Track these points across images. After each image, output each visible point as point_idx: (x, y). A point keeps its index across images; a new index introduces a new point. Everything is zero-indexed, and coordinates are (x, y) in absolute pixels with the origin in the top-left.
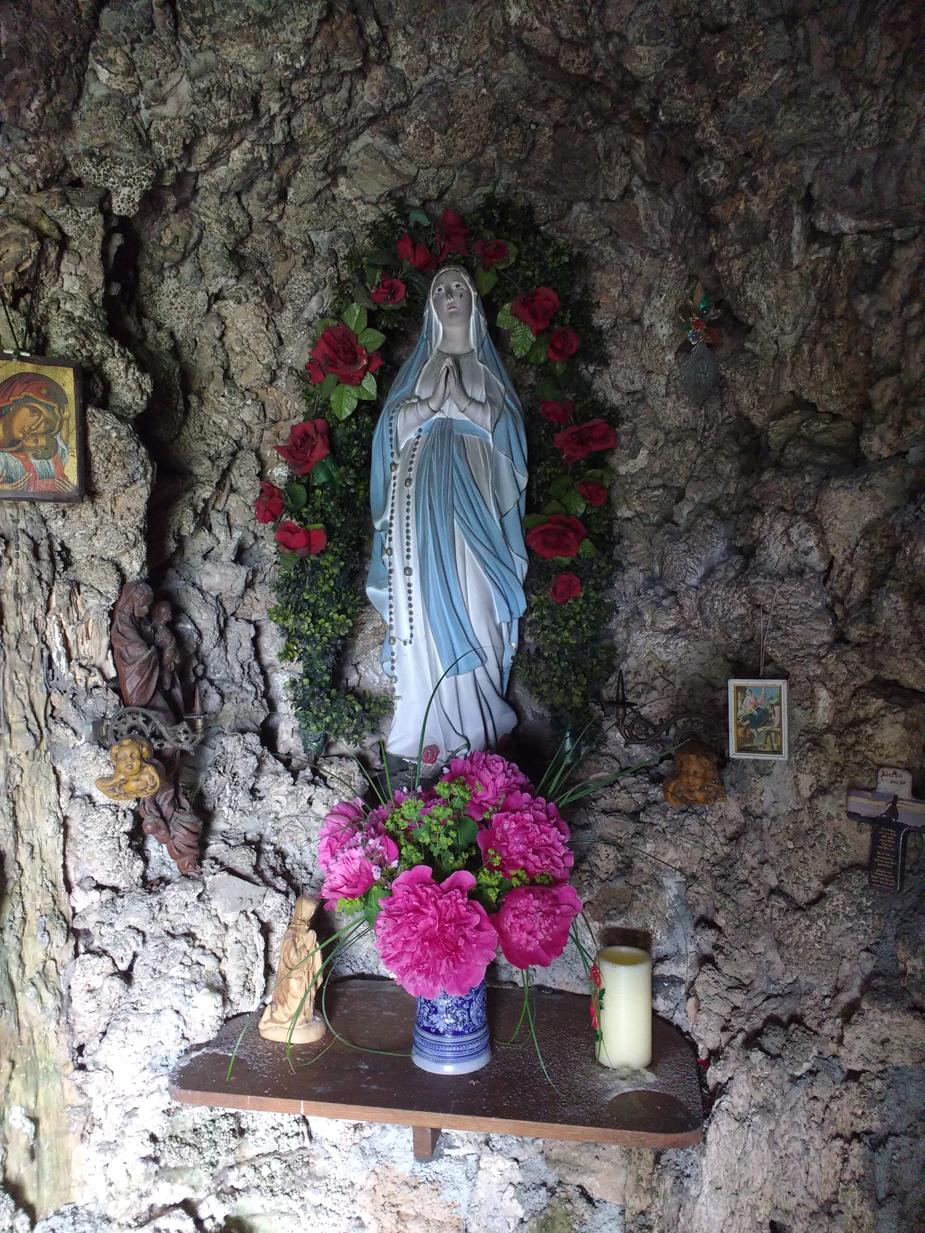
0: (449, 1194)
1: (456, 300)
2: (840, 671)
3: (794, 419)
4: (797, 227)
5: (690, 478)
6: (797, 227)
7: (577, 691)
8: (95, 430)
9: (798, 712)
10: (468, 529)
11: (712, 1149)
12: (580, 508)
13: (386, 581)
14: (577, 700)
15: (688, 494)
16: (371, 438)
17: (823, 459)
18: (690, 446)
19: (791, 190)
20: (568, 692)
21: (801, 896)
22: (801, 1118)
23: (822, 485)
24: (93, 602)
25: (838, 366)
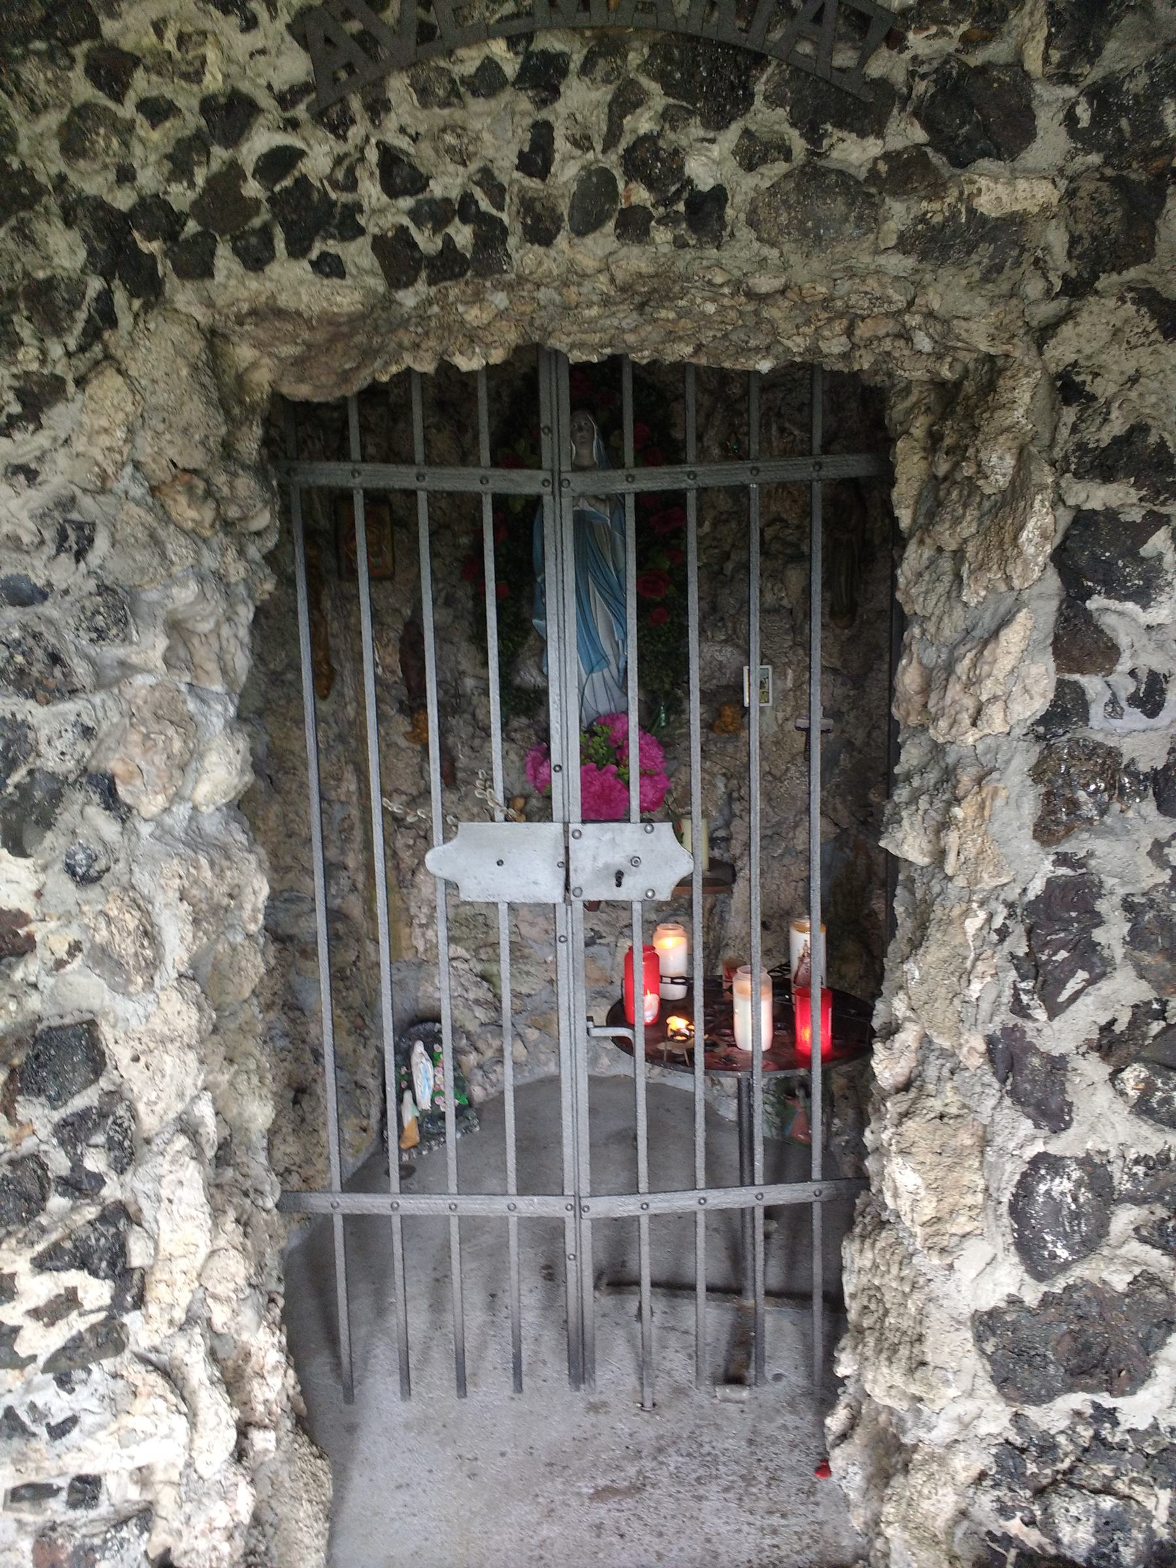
0: (600, 963)
1: (585, 433)
2: (794, 659)
3: (777, 526)
4: (774, 428)
5: (733, 546)
6: (774, 428)
7: (667, 680)
8: (397, 536)
9: (779, 682)
10: (595, 578)
11: (736, 895)
12: (667, 565)
13: (543, 616)
14: (667, 687)
15: (733, 556)
16: (532, 523)
17: (788, 551)
18: (734, 525)
19: (770, 408)
20: (662, 681)
21: (778, 773)
22: (776, 874)
23: (785, 565)
24: (392, 635)
25: (795, 501)
